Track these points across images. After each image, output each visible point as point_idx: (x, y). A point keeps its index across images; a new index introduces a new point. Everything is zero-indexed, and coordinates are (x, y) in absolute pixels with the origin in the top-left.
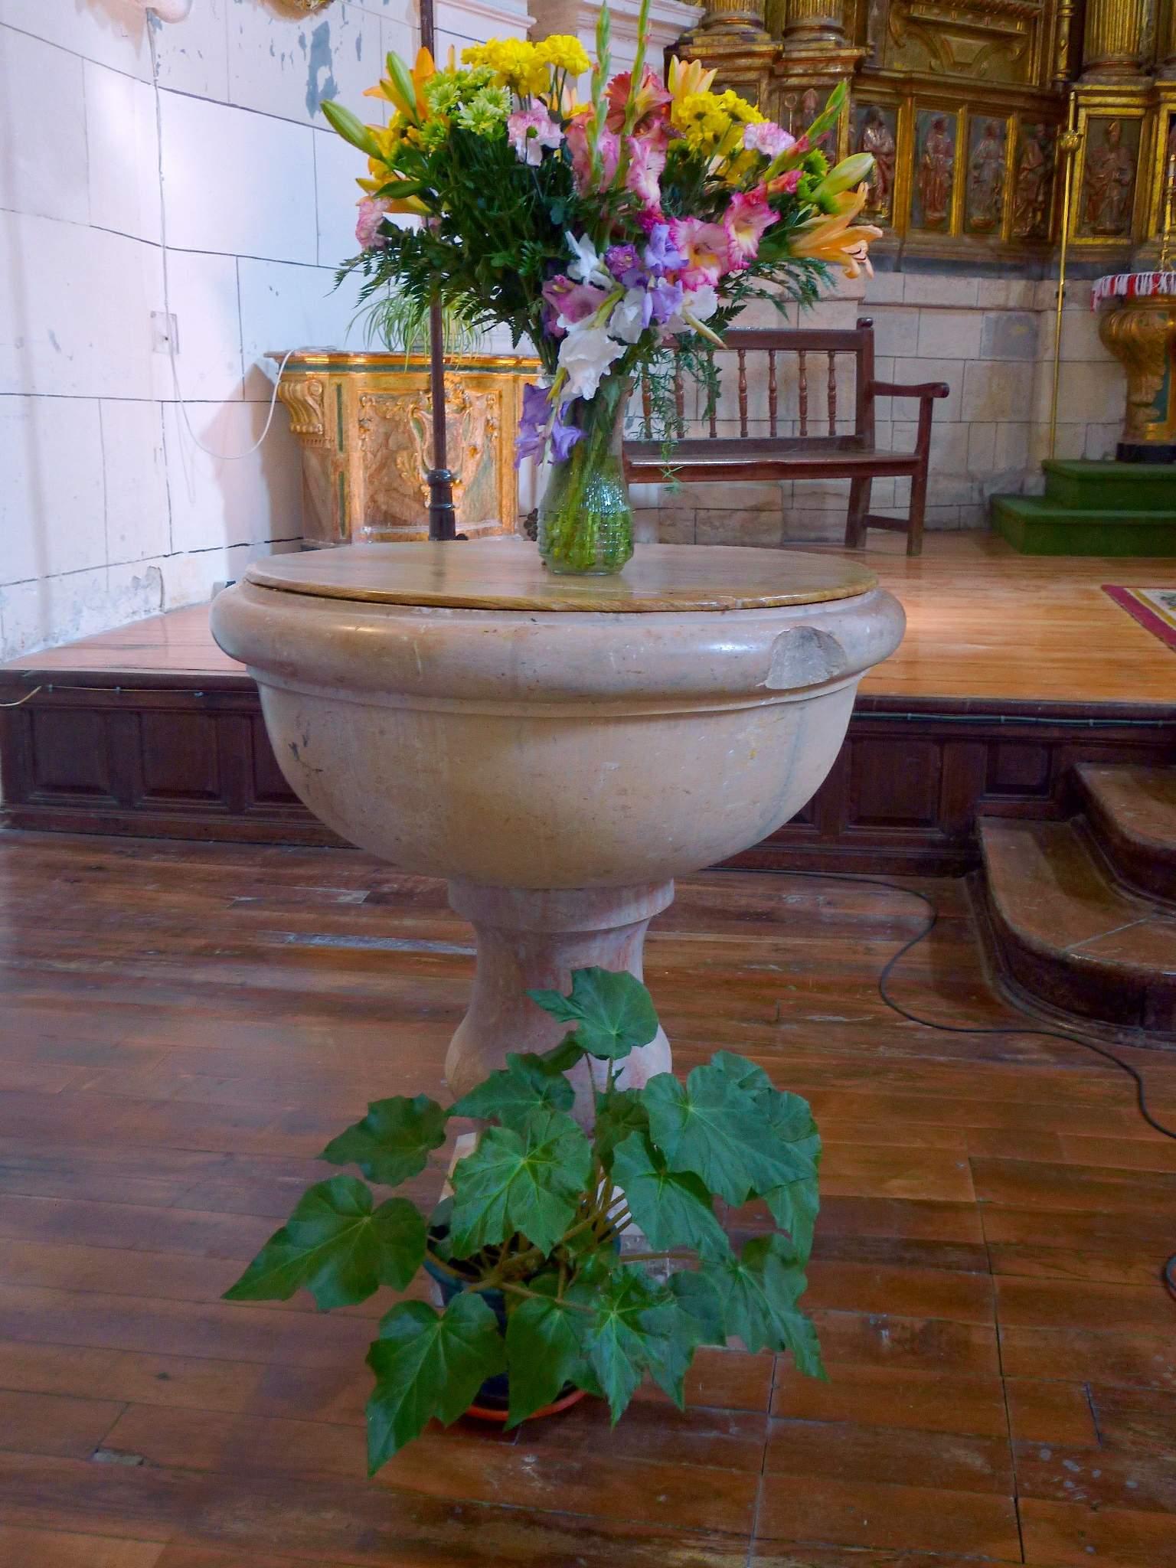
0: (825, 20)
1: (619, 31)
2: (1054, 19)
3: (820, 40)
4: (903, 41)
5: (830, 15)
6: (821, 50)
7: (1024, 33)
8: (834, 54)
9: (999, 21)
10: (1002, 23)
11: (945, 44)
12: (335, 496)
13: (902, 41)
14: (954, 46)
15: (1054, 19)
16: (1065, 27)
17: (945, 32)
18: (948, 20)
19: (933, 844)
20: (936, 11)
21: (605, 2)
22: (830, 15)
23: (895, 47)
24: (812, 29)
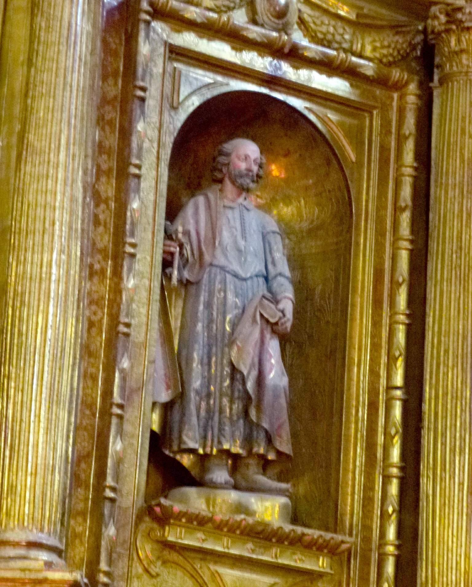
0: (35, 536)
1: (56, 154)
2: (374, 557)
3: (25, 558)
4: (157, 570)
5: (42, 530)
6: (23, 570)
7: (328, 570)
8: (40, 576)
9: (294, 553)
10: (296, 557)
11: (214, 575)
12: (58, 403)
13: (154, 570)
14: (228, 580)
15: (374, 557)
16: (390, 568)
17: (216, 563)
18: (219, 548)
19: (193, 72)
20: (200, 535)
21: (168, 2)
22: (42, 530)
23: (145, 577)
24: (16, 544)
